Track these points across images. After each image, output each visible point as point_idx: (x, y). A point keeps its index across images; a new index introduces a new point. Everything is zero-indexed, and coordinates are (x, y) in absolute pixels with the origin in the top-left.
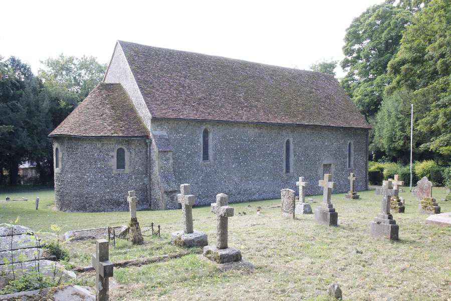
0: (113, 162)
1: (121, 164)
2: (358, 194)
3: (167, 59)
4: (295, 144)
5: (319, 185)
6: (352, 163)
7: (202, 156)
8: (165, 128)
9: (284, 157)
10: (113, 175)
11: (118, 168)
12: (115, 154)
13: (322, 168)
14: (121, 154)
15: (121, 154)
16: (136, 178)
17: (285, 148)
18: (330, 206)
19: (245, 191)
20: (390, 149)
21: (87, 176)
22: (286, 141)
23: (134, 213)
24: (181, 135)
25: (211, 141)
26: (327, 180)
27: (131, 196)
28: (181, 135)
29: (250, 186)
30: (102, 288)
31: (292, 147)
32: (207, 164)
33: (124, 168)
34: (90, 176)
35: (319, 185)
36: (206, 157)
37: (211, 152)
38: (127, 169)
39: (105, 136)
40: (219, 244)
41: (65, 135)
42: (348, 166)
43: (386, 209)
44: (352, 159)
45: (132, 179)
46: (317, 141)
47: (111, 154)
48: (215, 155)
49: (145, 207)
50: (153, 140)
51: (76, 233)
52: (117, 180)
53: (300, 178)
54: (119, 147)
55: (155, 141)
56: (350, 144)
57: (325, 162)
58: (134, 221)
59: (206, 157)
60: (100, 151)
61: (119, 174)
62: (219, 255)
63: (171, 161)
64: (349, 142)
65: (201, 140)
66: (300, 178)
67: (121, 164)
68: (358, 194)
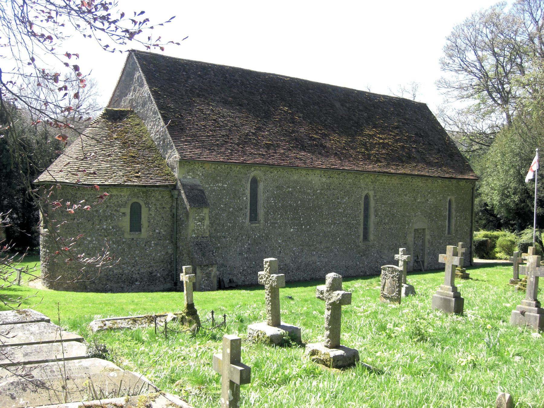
0: (125, 223)
1: (136, 226)
2: (468, 272)
3: (199, 76)
4: (376, 201)
5: (440, 261)
6: (453, 227)
7: (248, 214)
8: (199, 175)
9: (362, 217)
10: (124, 240)
11: (131, 231)
12: (127, 210)
13: (413, 235)
14: (136, 211)
15: (136, 211)
16: (155, 244)
17: (362, 205)
18: (454, 289)
19: (307, 265)
20: (501, 206)
21: (88, 240)
22: (364, 195)
23: (190, 296)
24: (220, 185)
25: (262, 195)
26: (451, 254)
27: (186, 274)
28: (220, 185)
29: (313, 258)
30: (232, 398)
31: (372, 204)
32: (256, 227)
33: (140, 231)
34: (91, 242)
35: (440, 261)
36: (254, 217)
37: (261, 212)
38: (145, 233)
39: (114, 185)
40: (328, 341)
41: (49, 181)
42: (447, 232)
43: (532, 295)
44: (453, 222)
45: (150, 246)
46: (406, 195)
47: (122, 210)
48: (267, 213)
49: (169, 285)
50: (182, 192)
51: (107, 322)
52: (130, 247)
53: (401, 249)
54: (135, 200)
55: (185, 193)
56: (450, 201)
57: (418, 226)
58: (191, 310)
59: (254, 217)
60: (107, 206)
61: (133, 239)
62: (332, 355)
63: (207, 222)
64: (449, 198)
65: (248, 192)
66: (401, 249)
67: (136, 226)
68: (468, 272)
